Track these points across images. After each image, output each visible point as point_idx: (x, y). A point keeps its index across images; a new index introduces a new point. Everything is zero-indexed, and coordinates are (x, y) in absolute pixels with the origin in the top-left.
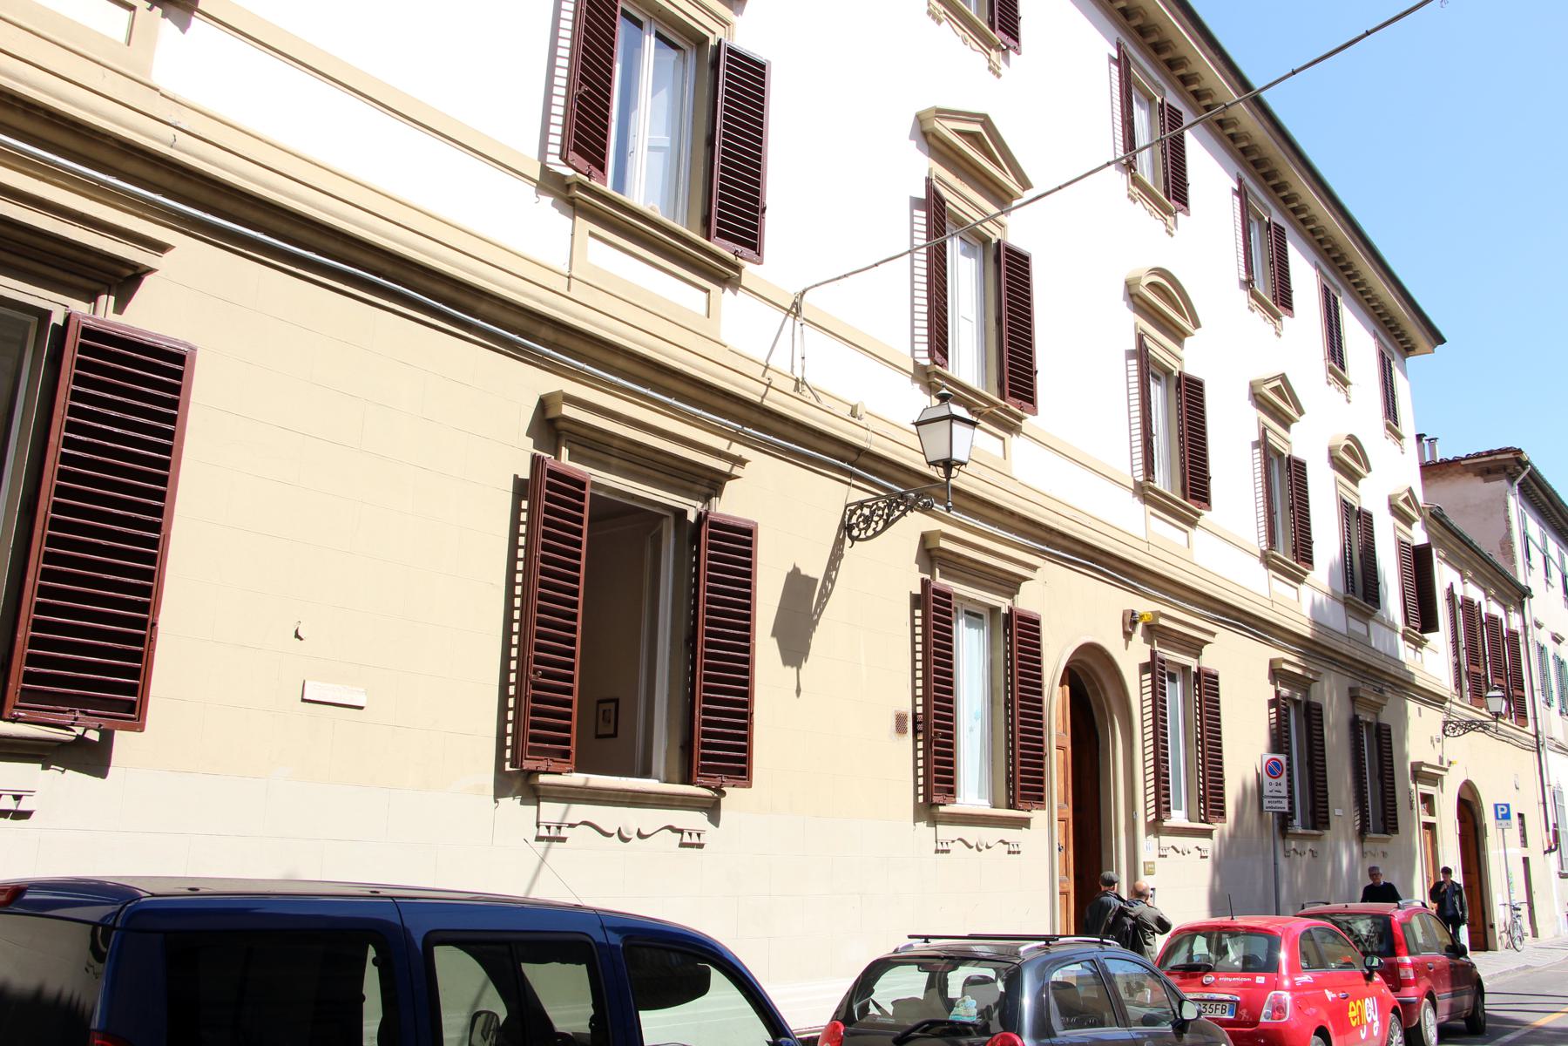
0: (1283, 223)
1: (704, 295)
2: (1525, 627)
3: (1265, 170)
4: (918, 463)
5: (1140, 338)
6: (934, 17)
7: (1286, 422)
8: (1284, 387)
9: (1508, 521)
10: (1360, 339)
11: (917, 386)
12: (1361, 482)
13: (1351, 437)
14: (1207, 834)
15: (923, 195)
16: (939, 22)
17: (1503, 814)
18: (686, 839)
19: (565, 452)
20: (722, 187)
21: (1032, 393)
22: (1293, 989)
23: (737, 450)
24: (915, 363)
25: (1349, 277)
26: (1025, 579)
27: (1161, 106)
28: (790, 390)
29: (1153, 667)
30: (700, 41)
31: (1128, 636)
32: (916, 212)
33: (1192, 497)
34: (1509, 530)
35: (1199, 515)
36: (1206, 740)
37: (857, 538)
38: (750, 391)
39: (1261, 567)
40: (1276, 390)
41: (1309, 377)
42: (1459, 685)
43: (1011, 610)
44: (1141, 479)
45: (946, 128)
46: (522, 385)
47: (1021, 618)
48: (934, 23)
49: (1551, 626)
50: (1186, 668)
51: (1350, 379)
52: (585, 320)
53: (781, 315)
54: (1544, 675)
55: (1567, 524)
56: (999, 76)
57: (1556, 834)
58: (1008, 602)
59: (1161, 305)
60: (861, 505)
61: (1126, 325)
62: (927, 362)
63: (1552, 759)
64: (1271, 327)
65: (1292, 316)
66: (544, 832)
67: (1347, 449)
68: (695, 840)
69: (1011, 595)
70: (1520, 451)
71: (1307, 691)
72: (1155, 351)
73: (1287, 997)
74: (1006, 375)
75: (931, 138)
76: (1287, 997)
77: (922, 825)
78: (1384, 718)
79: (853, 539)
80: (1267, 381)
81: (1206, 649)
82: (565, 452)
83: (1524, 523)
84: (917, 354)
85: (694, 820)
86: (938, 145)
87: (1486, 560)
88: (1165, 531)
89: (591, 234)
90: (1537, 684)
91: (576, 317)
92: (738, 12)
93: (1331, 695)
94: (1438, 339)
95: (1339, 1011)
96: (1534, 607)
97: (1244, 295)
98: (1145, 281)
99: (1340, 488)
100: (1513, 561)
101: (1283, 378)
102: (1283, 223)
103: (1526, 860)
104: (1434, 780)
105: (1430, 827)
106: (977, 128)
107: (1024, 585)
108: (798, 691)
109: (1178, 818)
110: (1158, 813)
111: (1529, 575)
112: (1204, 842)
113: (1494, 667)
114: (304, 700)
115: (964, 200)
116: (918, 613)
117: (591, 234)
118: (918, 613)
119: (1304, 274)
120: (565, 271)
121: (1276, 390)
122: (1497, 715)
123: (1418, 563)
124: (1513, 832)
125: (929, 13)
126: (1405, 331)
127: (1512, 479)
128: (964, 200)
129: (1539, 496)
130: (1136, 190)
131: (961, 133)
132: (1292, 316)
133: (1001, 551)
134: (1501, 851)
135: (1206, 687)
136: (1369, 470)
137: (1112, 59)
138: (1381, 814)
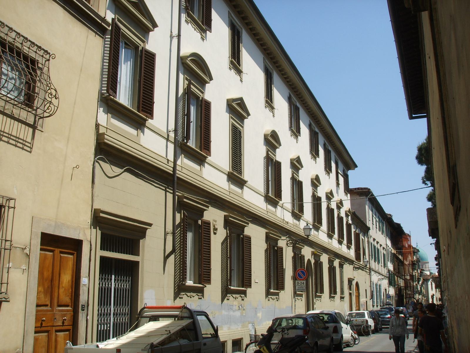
3: (239, 10)
6: (187, 22)
7: (203, 83)
8: (241, 102)
20: (143, 96)
21: (209, 148)
28: (282, 221)
30: (136, 47)
33: (142, 111)
37: (289, 246)
41: (255, 100)
49: (373, 237)
51: (275, 107)
53: (281, 208)
59: (195, 70)
70: (369, 189)
74: (141, 102)
75: (230, 106)
79: (288, 246)
86: (231, 107)
91: (148, 160)
99: (231, 120)
108: (366, 290)
114: (255, 282)
121: (238, 104)
127: (367, 196)
130: (267, 105)
132: (332, 173)
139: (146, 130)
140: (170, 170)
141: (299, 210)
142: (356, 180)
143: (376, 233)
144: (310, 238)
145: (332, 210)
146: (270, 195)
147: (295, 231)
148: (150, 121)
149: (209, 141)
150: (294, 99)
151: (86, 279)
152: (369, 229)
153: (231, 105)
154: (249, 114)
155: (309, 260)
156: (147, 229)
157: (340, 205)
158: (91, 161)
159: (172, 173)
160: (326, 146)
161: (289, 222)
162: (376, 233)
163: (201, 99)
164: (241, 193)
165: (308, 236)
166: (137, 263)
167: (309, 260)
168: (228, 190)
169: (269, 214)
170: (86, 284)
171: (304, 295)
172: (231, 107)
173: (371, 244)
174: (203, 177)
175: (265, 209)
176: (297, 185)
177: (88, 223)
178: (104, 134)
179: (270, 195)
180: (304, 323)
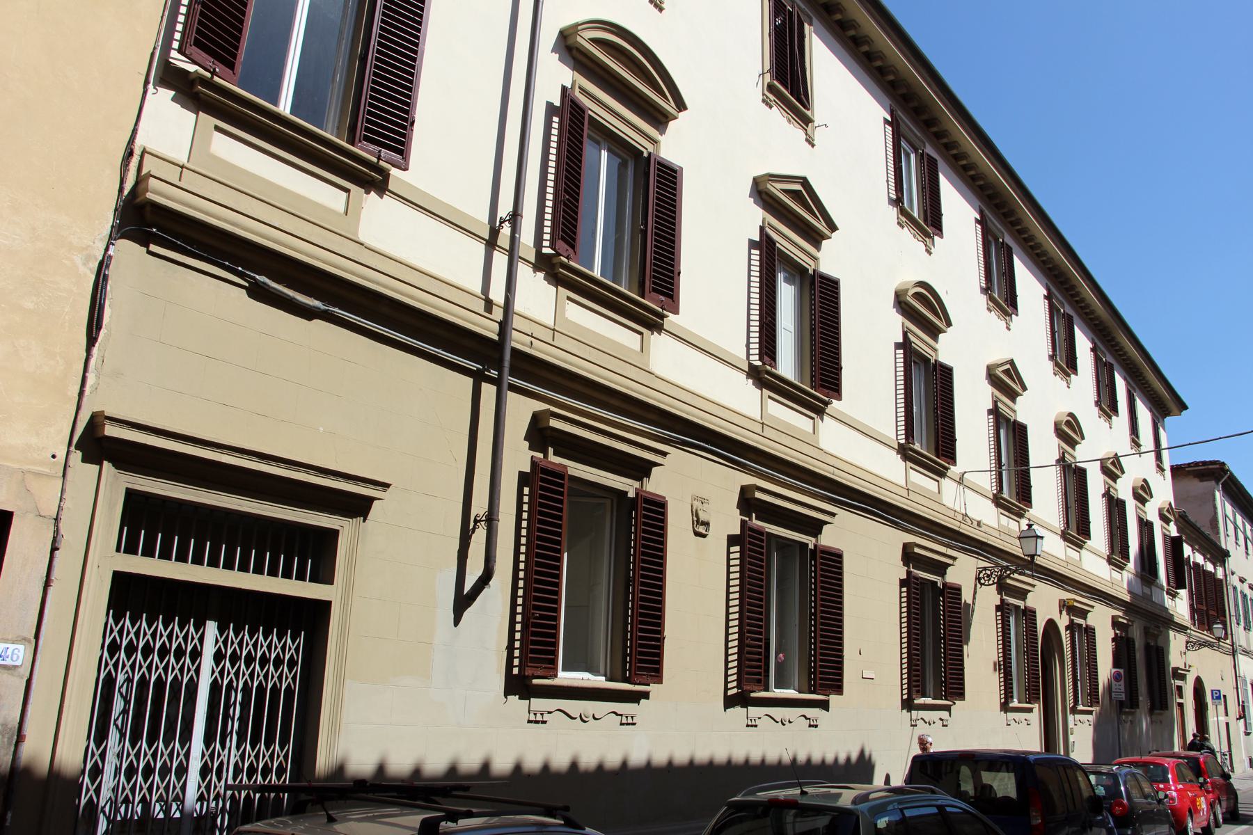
0: (1071, 312)
1: (344, 195)
2: (1226, 576)
4: (1019, 552)
5: (995, 403)
6: (767, 104)
7: (1013, 395)
8: (1012, 369)
9: (1215, 508)
10: (1144, 415)
11: (751, 381)
12: (1077, 447)
13: (1071, 415)
14: (1090, 713)
15: (758, 239)
16: (771, 107)
17: (1217, 696)
18: (624, 721)
19: (551, 450)
22: (1176, 790)
23: (1035, 582)
24: (750, 364)
25: (1072, 296)
26: (826, 523)
27: (922, 155)
29: (1071, 627)
31: (1061, 612)
32: (753, 251)
34: (1216, 513)
35: (827, 404)
36: (819, 614)
38: (953, 525)
39: (992, 506)
40: (1007, 372)
42: (1192, 618)
43: (815, 546)
44: (903, 442)
45: (776, 188)
46: (896, 538)
47: (822, 552)
48: (656, 11)
49: (1239, 573)
50: (1017, 607)
52: (354, 274)
53: (955, 484)
54: (1236, 605)
55: (1252, 509)
56: (813, 146)
57: (1243, 707)
58: (814, 540)
59: (922, 309)
60: (985, 569)
61: (894, 325)
62: (759, 363)
63: (1241, 658)
64: (1003, 323)
65: (941, 237)
66: (532, 718)
67: (1068, 423)
68: (630, 721)
69: (639, 479)
70: (1223, 464)
71: (1127, 632)
72: (782, 244)
73: (1174, 794)
76: (1174, 794)
77: (514, 699)
78: (1160, 643)
80: (999, 365)
81: (1029, 595)
82: (551, 450)
83: (1224, 507)
84: (751, 358)
85: (944, 714)
86: (770, 201)
87: (1206, 538)
88: (921, 480)
89: (569, 298)
90: (1233, 612)
91: (378, 283)
92: (662, 132)
93: (1136, 634)
94: (1183, 407)
95: (1194, 802)
96: (1231, 563)
97: (893, 212)
98: (911, 293)
100: (1218, 533)
101: (1012, 362)
102: (1071, 312)
103: (1227, 724)
104: (1183, 677)
105: (1181, 705)
106: (798, 187)
107: (655, 470)
109: (1015, 703)
110: (1006, 698)
111: (1227, 543)
112: (1090, 717)
113: (1212, 606)
115: (789, 242)
116: (904, 589)
117: (569, 298)
118: (904, 589)
119: (1083, 344)
120: (551, 323)
121: (1007, 372)
122: (1219, 639)
123: (1174, 546)
124: (1221, 708)
125: (763, 101)
126: (1166, 403)
128: (789, 242)
129: (1235, 492)
131: (785, 191)
132: (941, 237)
133: (629, 439)
134: (1215, 718)
135: (1090, 632)
136: (1083, 438)
137: (886, 121)
138: (1161, 700)
139: (825, 417)
140: (489, 329)
141: (1018, 494)
142: (1188, 437)
143: (1247, 553)
144: (1038, 561)
145: (1121, 504)
146: (1005, 495)
147: (565, 362)
148: (671, 317)
149: (672, 272)
150: (995, 223)
151: (21, 647)
152: (1226, 554)
153: (578, 49)
154: (1024, 388)
155: (1051, 624)
156: (370, 500)
157: (1142, 493)
158: (88, 258)
159: (496, 338)
160: (989, 223)
161: (985, 521)
162: (1247, 553)
163: (811, 272)
164: (638, 348)
165: (1032, 556)
166: (325, 606)
167: (1051, 624)
168: (758, 418)
169: (768, 432)
170: (19, 663)
171: (1036, 710)
172: (770, 201)
173: (1235, 588)
174: (362, 239)
175: (903, 484)
176: (1011, 436)
177: (54, 457)
178: (149, 175)
179: (1005, 495)
180: (1020, 786)
